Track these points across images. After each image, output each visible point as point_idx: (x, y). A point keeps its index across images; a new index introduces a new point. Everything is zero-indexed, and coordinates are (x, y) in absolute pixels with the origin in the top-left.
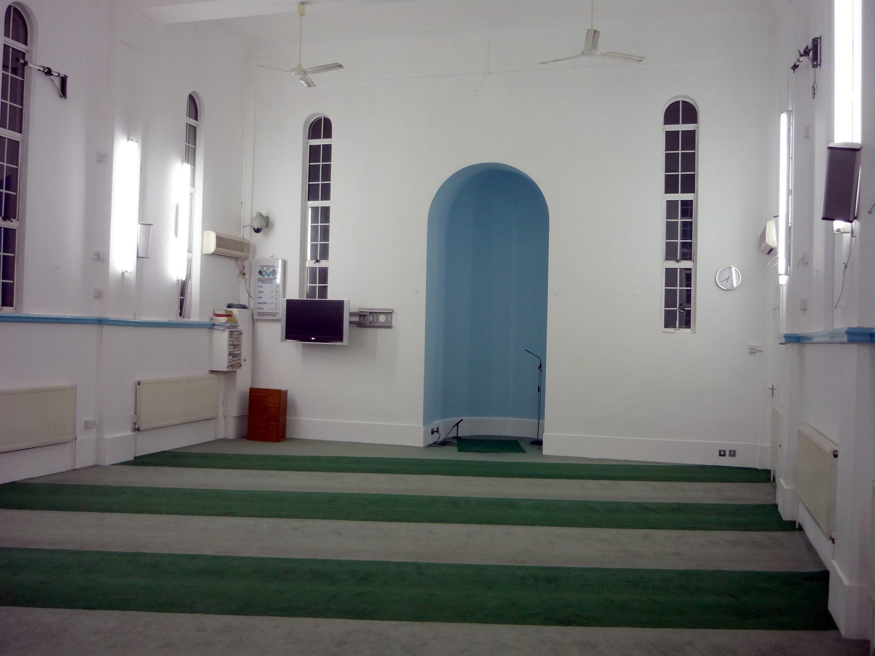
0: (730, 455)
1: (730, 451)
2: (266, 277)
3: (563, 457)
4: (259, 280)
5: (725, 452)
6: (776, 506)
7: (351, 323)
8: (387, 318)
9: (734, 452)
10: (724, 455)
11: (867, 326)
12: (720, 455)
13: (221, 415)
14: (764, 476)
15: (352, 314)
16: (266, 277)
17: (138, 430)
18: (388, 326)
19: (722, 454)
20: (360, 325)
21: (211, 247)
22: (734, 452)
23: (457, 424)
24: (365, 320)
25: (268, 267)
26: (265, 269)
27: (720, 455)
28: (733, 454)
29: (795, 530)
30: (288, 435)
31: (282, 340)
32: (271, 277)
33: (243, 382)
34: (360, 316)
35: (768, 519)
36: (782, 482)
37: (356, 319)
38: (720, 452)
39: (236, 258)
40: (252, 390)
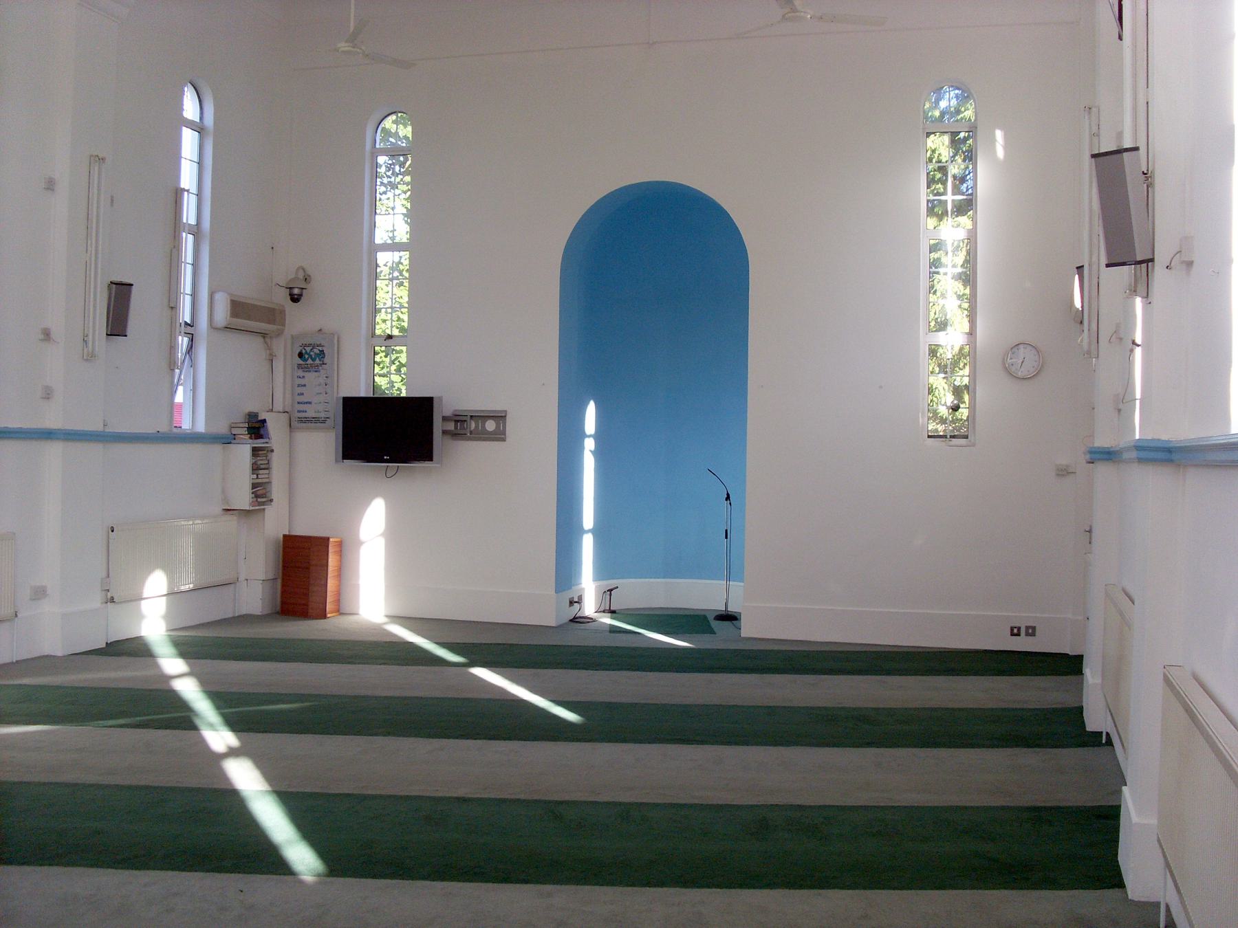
0: (1027, 634)
1: (1027, 628)
2: (310, 361)
3: (822, 643)
4: (299, 366)
5: (1019, 629)
6: (1080, 710)
7: (444, 432)
8: (498, 426)
9: (1034, 628)
10: (1018, 635)
11: (1164, 437)
12: (1013, 634)
13: (242, 578)
14: (1071, 665)
15: (445, 419)
16: (310, 361)
17: (112, 600)
18: (499, 435)
19: (1015, 632)
20: (455, 435)
21: (222, 314)
22: (1034, 628)
23: (611, 590)
24: (467, 426)
25: (314, 346)
26: (308, 349)
27: (1013, 634)
28: (1031, 631)
29: (1100, 744)
30: (145, 595)
31: (337, 461)
32: (317, 362)
33: (276, 523)
34: (457, 421)
35: (1067, 729)
36: (1091, 675)
37: (451, 426)
38: (1012, 629)
39: (264, 335)
40: (285, 536)
